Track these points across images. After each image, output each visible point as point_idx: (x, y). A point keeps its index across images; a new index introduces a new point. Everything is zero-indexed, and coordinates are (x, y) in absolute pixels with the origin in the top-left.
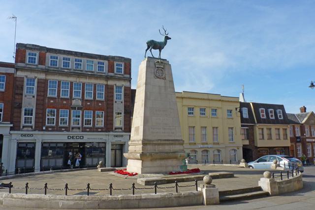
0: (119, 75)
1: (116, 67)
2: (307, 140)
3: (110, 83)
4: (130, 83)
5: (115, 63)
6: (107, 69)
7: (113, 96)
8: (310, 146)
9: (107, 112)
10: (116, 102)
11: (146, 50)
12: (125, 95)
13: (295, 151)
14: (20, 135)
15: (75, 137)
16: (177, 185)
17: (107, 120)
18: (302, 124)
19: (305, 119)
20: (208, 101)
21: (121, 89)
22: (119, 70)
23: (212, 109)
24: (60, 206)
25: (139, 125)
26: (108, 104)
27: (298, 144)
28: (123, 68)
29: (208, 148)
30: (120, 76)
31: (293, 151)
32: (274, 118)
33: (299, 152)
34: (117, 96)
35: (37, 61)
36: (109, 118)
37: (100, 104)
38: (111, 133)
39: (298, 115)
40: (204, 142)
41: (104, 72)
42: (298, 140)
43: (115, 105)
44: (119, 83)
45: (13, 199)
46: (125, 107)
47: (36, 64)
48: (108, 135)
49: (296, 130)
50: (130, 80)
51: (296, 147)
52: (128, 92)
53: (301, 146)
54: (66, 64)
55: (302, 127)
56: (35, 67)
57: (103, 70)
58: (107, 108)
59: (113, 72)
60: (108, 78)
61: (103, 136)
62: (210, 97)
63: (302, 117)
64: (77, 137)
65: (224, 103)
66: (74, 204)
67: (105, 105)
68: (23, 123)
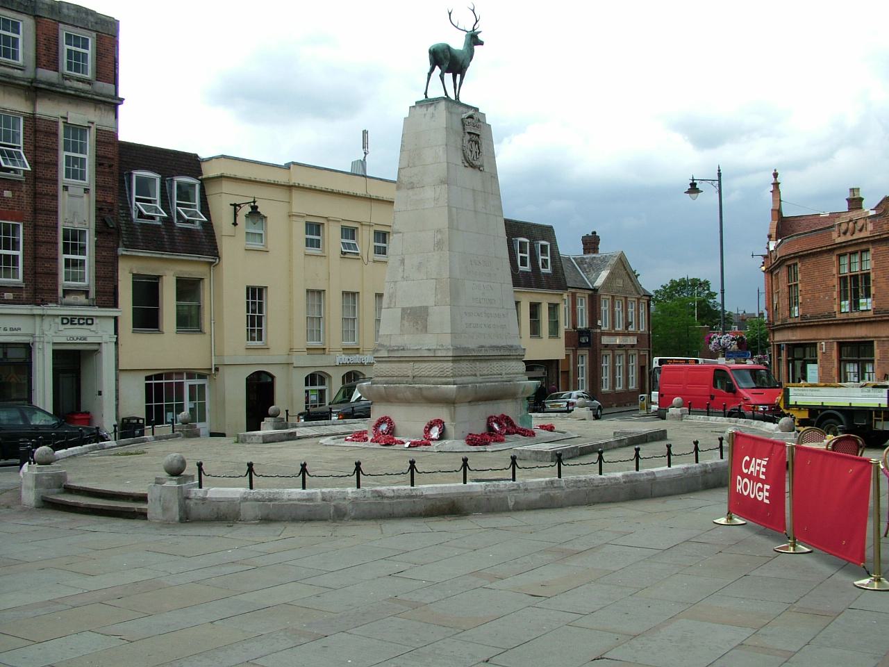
0: (79, 80)
1: (65, 48)
2: (605, 340)
3: (47, 109)
4: (116, 117)
5: (63, 31)
6: (32, 54)
7: (56, 164)
8: (609, 359)
9: (35, 227)
10: (66, 188)
11: (430, 75)
12: (100, 162)
13: (571, 374)
14: (58, 320)
15: (76, 321)
16: (600, 458)
17: (35, 258)
18: (595, 290)
19: (604, 274)
20: (364, 205)
21: (83, 137)
22: (77, 61)
23: (375, 232)
24: (511, 504)
25: (429, 301)
26: (35, 195)
27: (580, 352)
28: (90, 52)
29: (362, 364)
30: (80, 85)
31: (568, 372)
32: (528, 268)
33: (580, 378)
34: (68, 163)
35: (90, 64)
36: (42, 250)
37: (7, 194)
38: (52, 309)
39: (581, 262)
40: (350, 344)
41: (20, 61)
42: (583, 340)
43: (63, 198)
44: (78, 115)
45: (386, 501)
46: (99, 210)
47: (20, 61)
48: (42, 316)
49: (579, 307)
50: (112, 104)
51: (576, 363)
52: (111, 152)
53: (586, 359)
54: (77, 58)
55: (594, 296)
56: (86, 87)
57: (15, 57)
58: (35, 211)
59: (54, 65)
60: (34, 90)
61: (23, 319)
62: (297, 178)
63: (595, 267)
64: (81, 322)
65: (375, 206)
66: (541, 497)
67: (26, 199)
68: (63, 283)
